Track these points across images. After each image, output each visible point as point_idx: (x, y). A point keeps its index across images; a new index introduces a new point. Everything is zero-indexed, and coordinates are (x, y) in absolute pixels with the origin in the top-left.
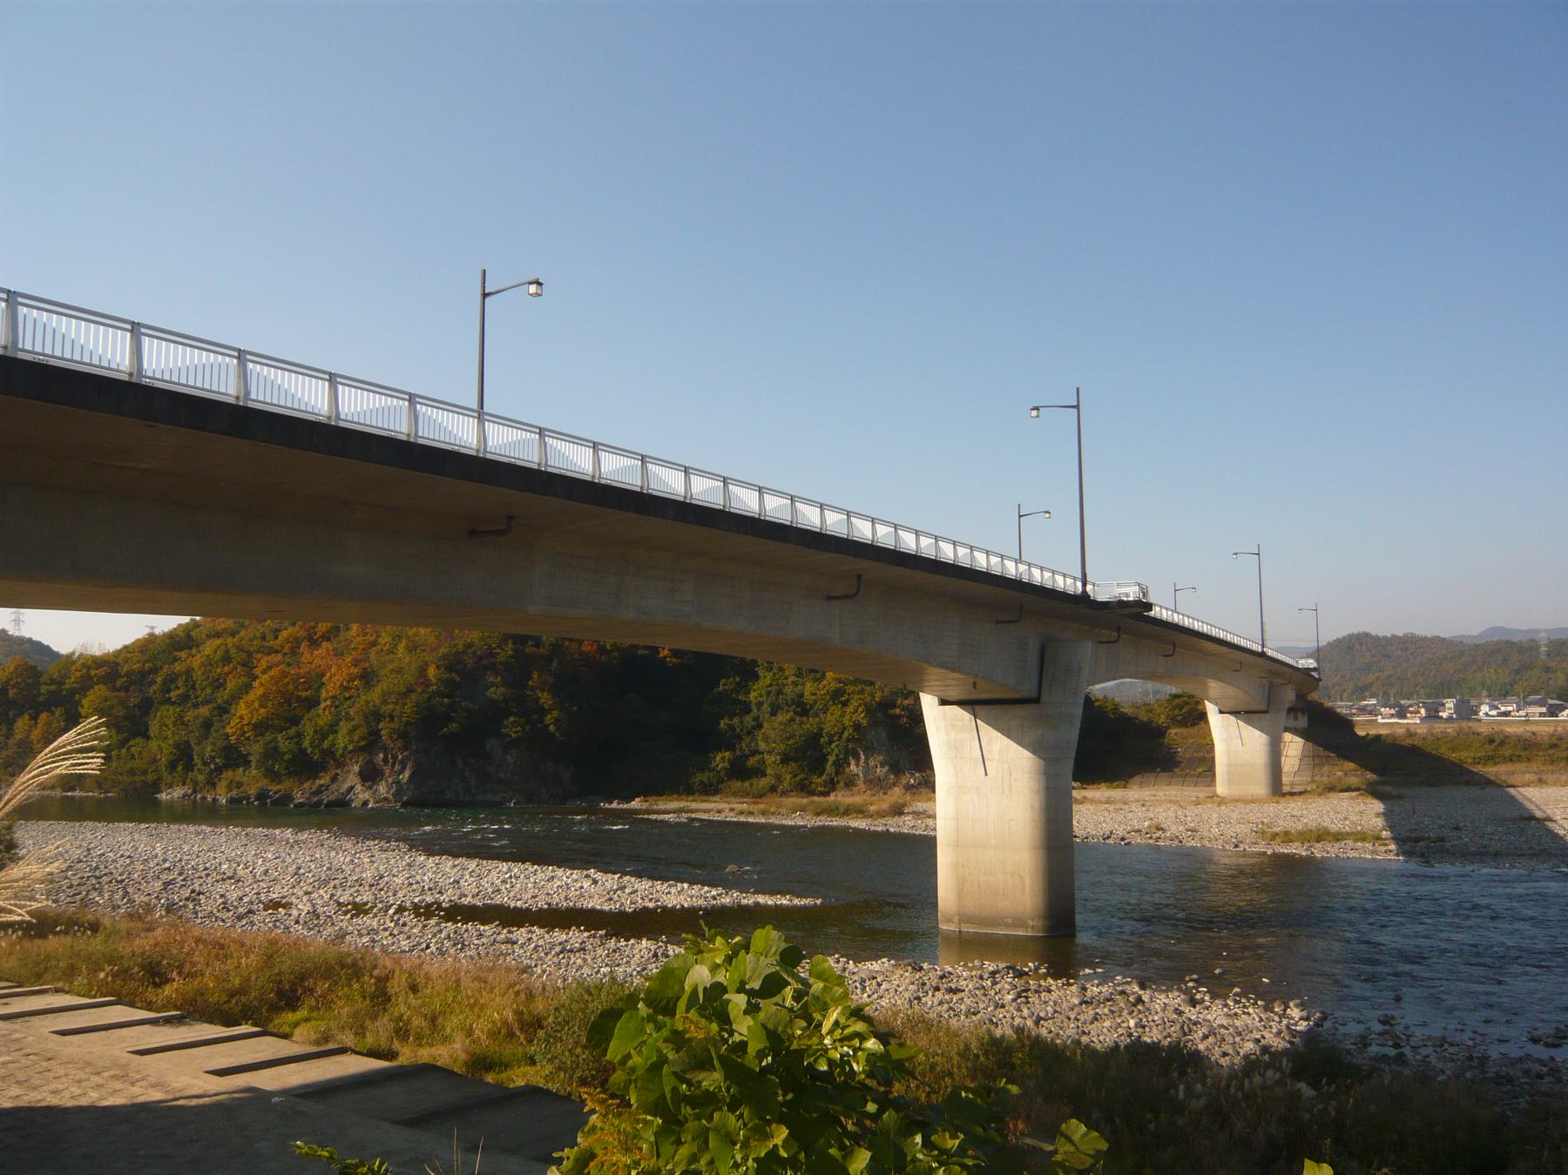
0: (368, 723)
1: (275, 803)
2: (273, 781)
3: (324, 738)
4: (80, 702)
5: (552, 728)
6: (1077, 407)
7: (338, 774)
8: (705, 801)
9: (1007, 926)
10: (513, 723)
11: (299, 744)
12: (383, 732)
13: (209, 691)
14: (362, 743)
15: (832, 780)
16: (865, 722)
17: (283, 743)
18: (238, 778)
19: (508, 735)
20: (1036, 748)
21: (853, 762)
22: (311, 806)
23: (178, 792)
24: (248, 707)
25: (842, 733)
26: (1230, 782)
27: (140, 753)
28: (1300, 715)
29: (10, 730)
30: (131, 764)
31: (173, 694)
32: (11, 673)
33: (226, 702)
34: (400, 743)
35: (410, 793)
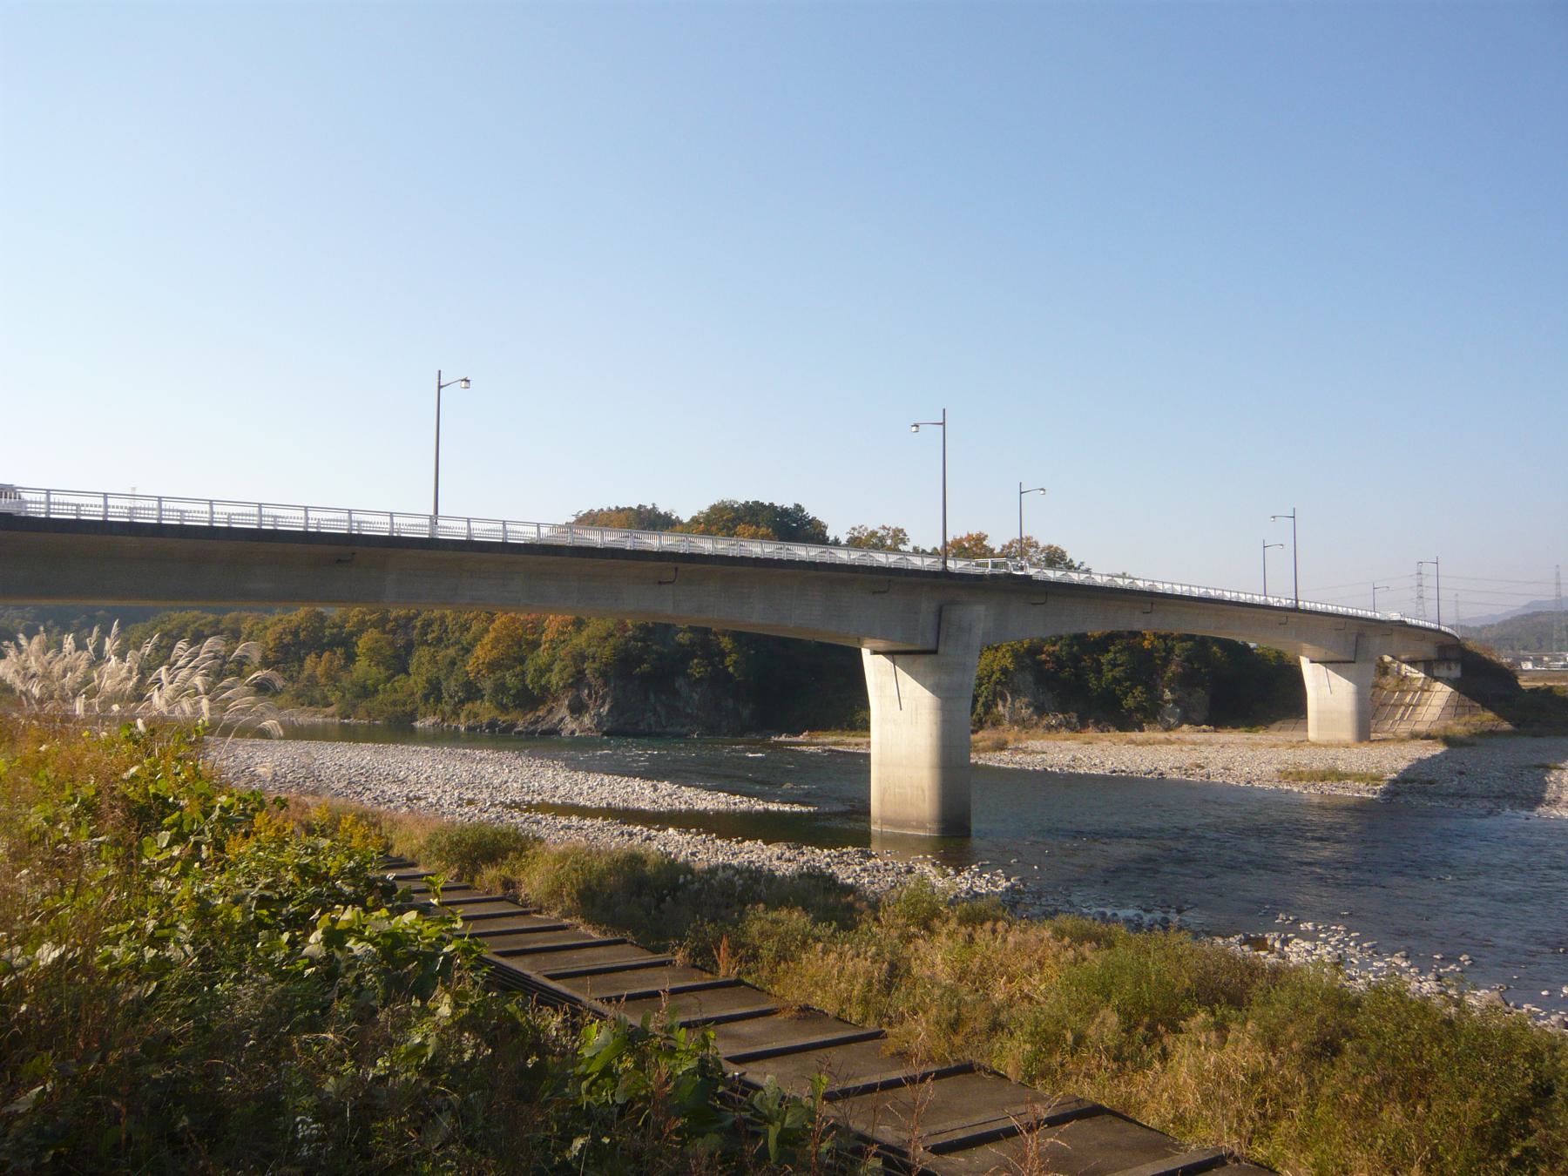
0: (575, 663)
1: (503, 731)
2: (502, 712)
3: (542, 676)
4: (356, 643)
5: (731, 669)
6: (944, 424)
9: (914, 828)
10: (697, 664)
13: (457, 634)
14: (570, 681)
15: (980, 720)
16: (1011, 667)
17: (510, 679)
19: (692, 675)
20: (935, 689)
21: (1000, 703)
23: (430, 721)
25: (991, 676)
26: (1319, 728)
27: (402, 687)
28: (1453, 666)
29: (301, 666)
30: (394, 697)
31: (429, 637)
32: (302, 619)
33: (470, 644)
34: (600, 681)
35: (609, 724)
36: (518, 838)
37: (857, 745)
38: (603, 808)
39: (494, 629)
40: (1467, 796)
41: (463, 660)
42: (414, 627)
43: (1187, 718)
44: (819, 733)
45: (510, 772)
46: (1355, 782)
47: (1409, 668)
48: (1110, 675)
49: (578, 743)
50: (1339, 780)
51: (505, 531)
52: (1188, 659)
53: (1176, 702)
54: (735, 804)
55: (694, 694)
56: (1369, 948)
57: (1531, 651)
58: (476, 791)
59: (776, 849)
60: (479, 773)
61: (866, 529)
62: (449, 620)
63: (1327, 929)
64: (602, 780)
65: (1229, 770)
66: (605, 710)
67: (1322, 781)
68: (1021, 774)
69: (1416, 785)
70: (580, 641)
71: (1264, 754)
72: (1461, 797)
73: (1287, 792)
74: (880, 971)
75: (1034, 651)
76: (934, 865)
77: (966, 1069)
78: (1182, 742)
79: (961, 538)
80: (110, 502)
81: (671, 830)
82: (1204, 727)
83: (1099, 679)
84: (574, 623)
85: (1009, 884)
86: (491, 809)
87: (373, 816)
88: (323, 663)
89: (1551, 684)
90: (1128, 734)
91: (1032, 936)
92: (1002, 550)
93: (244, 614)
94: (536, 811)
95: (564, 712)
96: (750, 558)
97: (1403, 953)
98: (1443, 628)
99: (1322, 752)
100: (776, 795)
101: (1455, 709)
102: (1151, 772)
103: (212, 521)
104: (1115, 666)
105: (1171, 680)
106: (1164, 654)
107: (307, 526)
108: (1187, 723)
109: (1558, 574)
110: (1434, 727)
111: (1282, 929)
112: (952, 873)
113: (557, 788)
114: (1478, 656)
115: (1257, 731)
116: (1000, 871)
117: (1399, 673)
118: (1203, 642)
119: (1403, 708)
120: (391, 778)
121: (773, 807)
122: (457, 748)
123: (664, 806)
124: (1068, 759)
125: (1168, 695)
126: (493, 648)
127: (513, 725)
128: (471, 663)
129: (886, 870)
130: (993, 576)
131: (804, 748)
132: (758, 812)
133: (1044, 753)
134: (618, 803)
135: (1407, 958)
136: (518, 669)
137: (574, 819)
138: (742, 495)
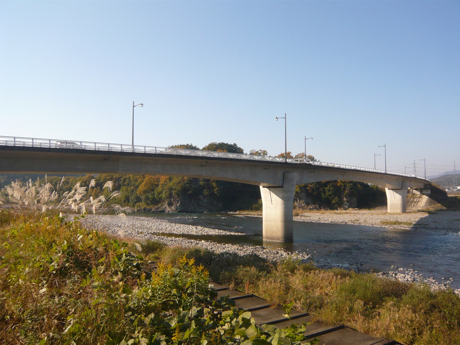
3: (160, 195)
5: (216, 192)
6: (285, 118)
7: (163, 204)
8: (256, 212)
9: (276, 240)
11: (154, 196)
12: (173, 193)
13: (134, 182)
14: (168, 196)
16: (299, 191)
17: (150, 196)
18: (140, 205)
20: (282, 198)
21: (296, 202)
22: (155, 212)
24: (142, 187)
28: (428, 190)
31: (126, 183)
32: (87, 178)
33: (138, 185)
34: (177, 196)
35: (180, 209)
36: (160, 244)
37: (254, 215)
38: (181, 234)
39: (145, 181)
40: (438, 229)
41: (136, 190)
42: (121, 181)
43: (350, 206)
44: (242, 211)
45: (152, 223)
46: (404, 225)
47: (415, 191)
48: (328, 194)
49: (169, 215)
50: (399, 224)
51: (156, 150)
52: (351, 189)
53: (347, 201)
54: (221, 233)
55: (205, 200)
56: (422, 276)
57: (446, 186)
58: (142, 229)
59: (236, 247)
60: (143, 224)
61: (255, 151)
62: (131, 178)
63: (407, 270)
64: (180, 226)
65: (366, 221)
66: (178, 205)
67: (394, 224)
68: (304, 223)
69: (422, 225)
70: (171, 184)
71: (375, 217)
72: (436, 229)
73: (384, 228)
74: (283, 287)
75: (306, 186)
76: (284, 251)
77: (342, 327)
78: (350, 213)
79: (283, 153)
80: (34, 141)
81: (203, 241)
82: (356, 209)
83: (325, 195)
84: (169, 179)
85: (308, 257)
86: (148, 235)
87: (114, 238)
88: (94, 191)
89: (457, 196)
90: (334, 211)
91: (326, 275)
92: (295, 157)
93: (70, 177)
94: (161, 235)
95: (166, 205)
96: (229, 158)
97: (432, 277)
98: (426, 179)
99: (392, 216)
100: (233, 230)
101: (429, 203)
102: (342, 223)
103: (50, 146)
104: (329, 191)
105: (346, 195)
106: (344, 187)
107: (96, 148)
108: (351, 207)
109: (455, 163)
110: (423, 208)
111: (393, 270)
112: (290, 253)
113: (167, 228)
114: (436, 187)
115: (371, 210)
116: (304, 253)
117: (412, 192)
118: (355, 184)
119: (414, 203)
120: (116, 226)
121: (233, 234)
122: (135, 216)
123: (200, 233)
124: (317, 218)
125: (345, 199)
126: (145, 186)
127: (151, 210)
128: (138, 191)
129: (270, 253)
130: (300, 164)
131: (238, 216)
132: (228, 235)
133: (310, 217)
134: (186, 233)
135: (434, 279)
136: (152, 193)
137: (173, 238)
138: (218, 141)
